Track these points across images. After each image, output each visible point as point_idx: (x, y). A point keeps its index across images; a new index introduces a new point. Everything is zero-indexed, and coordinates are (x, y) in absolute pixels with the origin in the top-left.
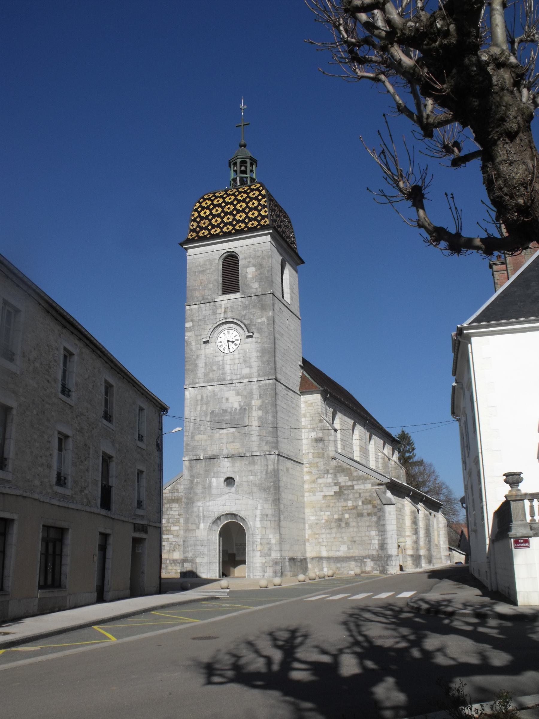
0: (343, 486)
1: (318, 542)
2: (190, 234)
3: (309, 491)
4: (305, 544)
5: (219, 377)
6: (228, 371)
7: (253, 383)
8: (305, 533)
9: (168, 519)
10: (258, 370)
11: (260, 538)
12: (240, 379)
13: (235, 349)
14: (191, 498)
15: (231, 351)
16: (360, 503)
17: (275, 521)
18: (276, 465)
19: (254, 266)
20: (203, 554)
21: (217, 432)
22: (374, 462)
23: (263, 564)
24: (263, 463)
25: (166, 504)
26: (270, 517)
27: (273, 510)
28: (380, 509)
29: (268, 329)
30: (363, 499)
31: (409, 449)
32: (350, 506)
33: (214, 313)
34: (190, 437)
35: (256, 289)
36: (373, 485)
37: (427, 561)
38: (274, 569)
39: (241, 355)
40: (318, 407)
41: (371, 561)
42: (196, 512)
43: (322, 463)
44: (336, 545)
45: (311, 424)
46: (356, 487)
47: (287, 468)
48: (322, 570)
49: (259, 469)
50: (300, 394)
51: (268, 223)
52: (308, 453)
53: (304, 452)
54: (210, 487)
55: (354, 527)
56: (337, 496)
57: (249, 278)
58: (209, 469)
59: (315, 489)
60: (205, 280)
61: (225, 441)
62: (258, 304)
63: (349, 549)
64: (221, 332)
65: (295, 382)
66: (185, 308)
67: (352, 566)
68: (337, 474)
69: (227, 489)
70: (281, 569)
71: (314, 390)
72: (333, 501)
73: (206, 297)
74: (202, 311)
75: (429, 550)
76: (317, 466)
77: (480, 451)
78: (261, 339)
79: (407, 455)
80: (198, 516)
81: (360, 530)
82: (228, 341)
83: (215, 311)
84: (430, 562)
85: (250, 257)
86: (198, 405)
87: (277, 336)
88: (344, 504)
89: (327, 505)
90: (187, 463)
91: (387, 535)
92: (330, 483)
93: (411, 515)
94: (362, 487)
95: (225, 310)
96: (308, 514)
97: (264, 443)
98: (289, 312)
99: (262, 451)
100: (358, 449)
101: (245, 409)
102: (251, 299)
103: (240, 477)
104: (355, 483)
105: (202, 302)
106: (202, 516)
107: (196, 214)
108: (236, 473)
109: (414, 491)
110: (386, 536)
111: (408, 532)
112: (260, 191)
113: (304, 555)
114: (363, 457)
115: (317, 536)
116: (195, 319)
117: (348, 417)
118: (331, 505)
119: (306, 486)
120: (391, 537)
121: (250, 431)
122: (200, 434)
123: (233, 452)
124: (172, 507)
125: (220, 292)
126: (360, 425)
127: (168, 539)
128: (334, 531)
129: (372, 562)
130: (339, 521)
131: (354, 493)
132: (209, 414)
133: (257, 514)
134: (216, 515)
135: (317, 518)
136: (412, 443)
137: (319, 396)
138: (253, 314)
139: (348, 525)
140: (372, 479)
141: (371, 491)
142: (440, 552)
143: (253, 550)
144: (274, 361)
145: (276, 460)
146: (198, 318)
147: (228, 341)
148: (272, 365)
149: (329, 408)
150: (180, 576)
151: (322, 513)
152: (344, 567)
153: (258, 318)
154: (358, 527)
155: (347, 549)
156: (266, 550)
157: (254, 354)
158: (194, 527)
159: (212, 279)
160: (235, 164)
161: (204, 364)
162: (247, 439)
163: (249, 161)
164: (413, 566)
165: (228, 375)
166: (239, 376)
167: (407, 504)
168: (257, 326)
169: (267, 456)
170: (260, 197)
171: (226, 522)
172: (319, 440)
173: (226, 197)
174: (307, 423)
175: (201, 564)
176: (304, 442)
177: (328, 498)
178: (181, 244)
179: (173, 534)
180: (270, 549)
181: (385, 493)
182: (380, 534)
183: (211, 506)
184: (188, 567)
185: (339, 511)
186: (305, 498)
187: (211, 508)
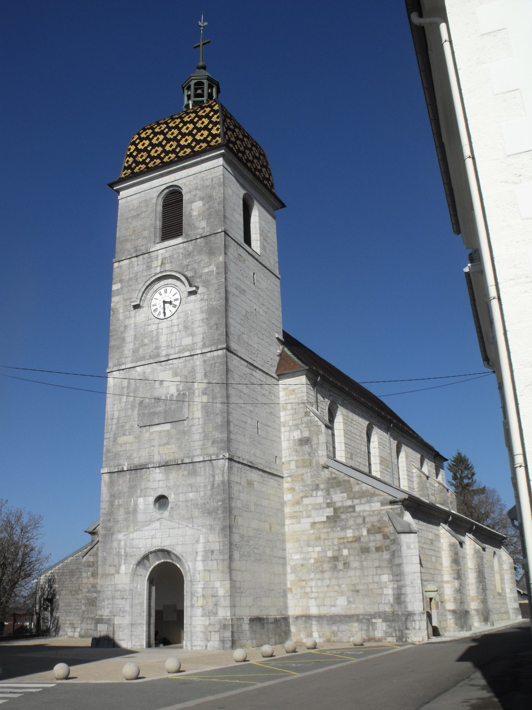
0: (340, 508)
1: (304, 592)
2: (124, 173)
4: (285, 596)
5: (152, 353)
7: (196, 357)
8: (285, 580)
10: (203, 338)
11: (202, 586)
12: (179, 352)
13: (173, 312)
14: (111, 528)
16: (365, 533)
17: (224, 560)
18: (226, 476)
19: (202, 199)
20: (124, 611)
21: (147, 431)
22: (406, 481)
23: (206, 627)
24: (207, 473)
26: (216, 555)
27: (222, 544)
28: (394, 540)
29: (218, 280)
30: (369, 525)
31: (467, 474)
32: (350, 537)
33: (149, 267)
34: (111, 439)
35: (203, 228)
36: (383, 504)
37: (482, 618)
38: (221, 636)
39: (181, 320)
40: (302, 394)
41: (383, 621)
43: (309, 474)
44: (330, 597)
46: (358, 509)
47: (248, 481)
48: (310, 635)
49: (203, 481)
50: (277, 377)
52: (290, 461)
53: (284, 460)
54: (135, 511)
55: (356, 568)
56: (331, 522)
58: (134, 485)
59: (300, 514)
60: (139, 226)
61: (156, 443)
62: (204, 249)
63: (349, 602)
64: (155, 292)
66: (113, 266)
67: (354, 630)
69: (157, 514)
70: (233, 636)
71: (295, 370)
72: (325, 530)
73: (139, 248)
74: (133, 267)
75: (484, 601)
77: (493, 292)
78: (208, 294)
79: (466, 481)
80: (119, 555)
81: (366, 574)
82: (165, 302)
83: (150, 264)
84: (486, 619)
85: (196, 189)
87: (231, 289)
88: (342, 534)
89: (316, 537)
90: (106, 477)
91: (404, 580)
92: (320, 504)
94: (367, 507)
95: (162, 261)
96: (290, 551)
97: (210, 443)
100: (378, 461)
101: (184, 394)
102: (196, 242)
103: (176, 494)
104: (356, 501)
105: (134, 255)
106: (123, 554)
108: (170, 489)
109: (477, 525)
111: (447, 574)
113: (283, 612)
115: (304, 583)
116: (124, 278)
117: (358, 415)
118: (323, 536)
119: (287, 510)
120: (412, 583)
121: (190, 426)
122: (124, 434)
126: (380, 428)
128: (327, 575)
129: (384, 624)
130: (334, 561)
131: (356, 517)
132: (137, 406)
134: (143, 552)
136: (471, 467)
137: (303, 379)
138: (199, 262)
139: (347, 566)
140: (382, 496)
141: (380, 513)
142: (506, 603)
143: (192, 606)
144: (224, 323)
145: (226, 467)
146: (128, 277)
147: (165, 302)
148: (223, 330)
149: (324, 398)
150: (92, 644)
151: (310, 549)
152: (342, 631)
153: (204, 267)
154: (362, 568)
155: (346, 603)
157: (199, 317)
158: (112, 570)
159: (148, 225)
160: (189, 88)
161: (133, 337)
163: (206, 82)
164: (457, 627)
165: (163, 348)
166: (177, 349)
167: (444, 533)
168: (203, 277)
169: (214, 462)
171: (157, 563)
174: (288, 418)
175: (120, 627)
176: (285, 445)
177: (318, 526)
178: (111, 185)
180: (216, 605)
181: (401, 515)
182: (395, 579)
183: (136, 539)
184: (102, 630)
185: (334, 545)
186: (286, 527)
187: (135, 542)
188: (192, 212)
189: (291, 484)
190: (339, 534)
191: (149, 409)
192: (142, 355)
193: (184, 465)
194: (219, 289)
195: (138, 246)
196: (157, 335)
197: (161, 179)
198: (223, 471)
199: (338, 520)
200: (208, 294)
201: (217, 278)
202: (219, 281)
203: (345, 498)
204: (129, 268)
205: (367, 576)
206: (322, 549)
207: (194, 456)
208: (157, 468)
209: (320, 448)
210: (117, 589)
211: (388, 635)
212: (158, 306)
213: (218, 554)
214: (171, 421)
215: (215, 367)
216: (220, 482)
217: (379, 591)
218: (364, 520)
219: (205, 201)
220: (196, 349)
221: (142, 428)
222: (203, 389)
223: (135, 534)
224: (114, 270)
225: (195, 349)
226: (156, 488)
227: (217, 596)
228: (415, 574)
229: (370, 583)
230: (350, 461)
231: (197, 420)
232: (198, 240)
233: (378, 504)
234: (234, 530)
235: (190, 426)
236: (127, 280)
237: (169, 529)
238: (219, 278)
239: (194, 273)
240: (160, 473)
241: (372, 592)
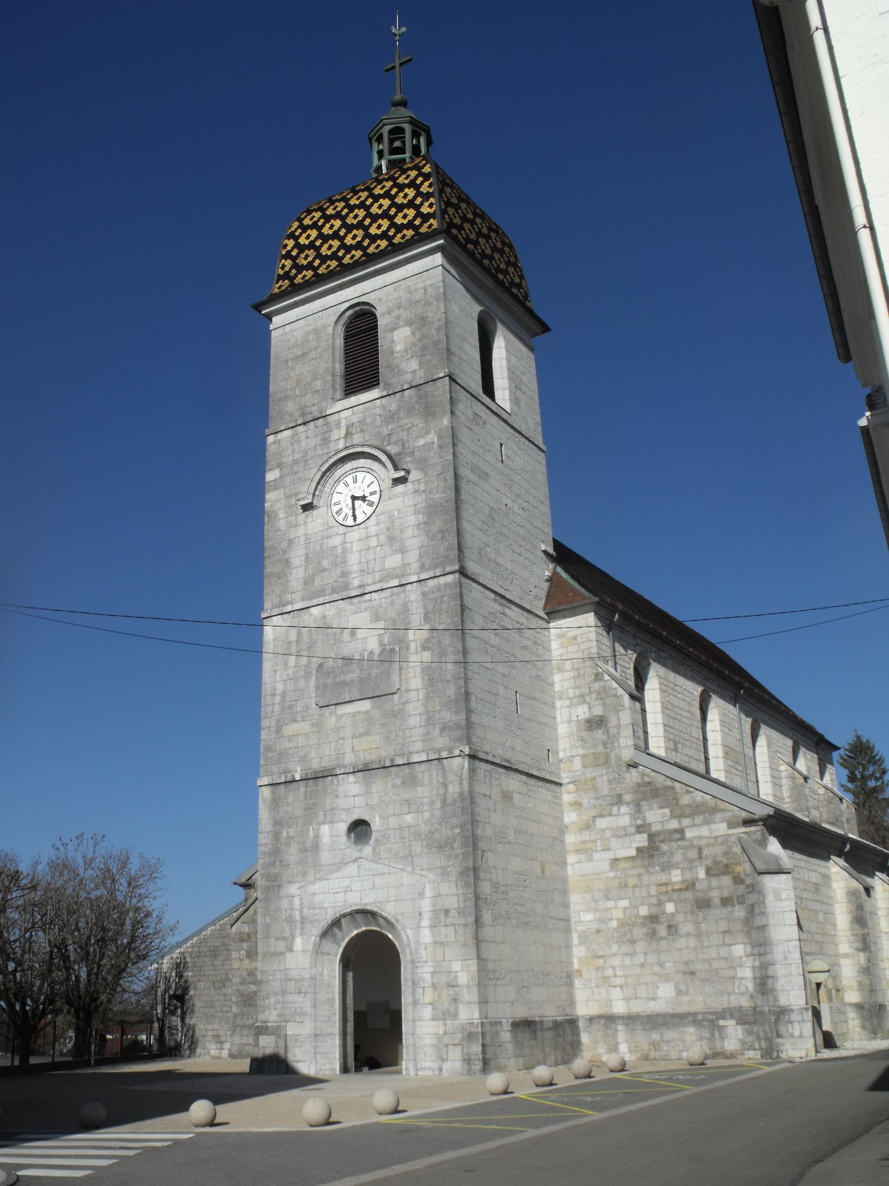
0: (658, 833)
1: (603, 977)
2: (277, 286)
3: (577, 851)
5: (336, 584)
7: (409, 587)
8: (570, 956)
10: (421, 556)
11: (430, 970)
12: (381, 581)
14: (277, 876)
15: (359, 521)
16: (702, 874)
17: (466, 925)
18: (465, 784)
19: (409, 323)
21: (331, 713)
22: (769, 785)
23: (439, 1038)
24: (435, 781)
26: (454, 918)
27: (461, 899)
29: (441, 457)
30: (708, 862)
31: (874, 772)
32: (677, 883)
33: (325, 441)
34: (273, 729)
35: (414, 372)
36: (731, 825)
38: (465, 1051)
39: (382, 526)
41: (737, 1024)
42: (286, 911)
43: (605, 778)
44: (646, 984)
45: (576, 688)
46: (689, 834)
48: (614, 1049)
49: (427, 794)
50: (546, 617)
52: (573, 756)
53: (561, 755)
54: (316, 847)
55: (688, 935)
57: (397, 352)
58: (314, 804)
59: (592, 845)
61: (348, 732)
62: (417, 406)
63: (679, 992)
64: (338, 481)
65: (531, 587)
66: (265, 440)
67: (688, 1038)
68: (642, 803)
69: (353, 851)
70: (484, 1051)
71: (576, 604)
72: (634, 872)
73: (308, 410)
76: (595, 788)
79: (872, 784)
80: (290, 920)
81: (706, 943)
82: (354, 498)
85: (399, 308)
87: (464, 472)
88: (664, 878)
90: (266, 793)
91: (771, 953)
92: (625, 828)
93: (849, 902)
94: (704, 831)
96: (577, 908)
97: (437, 731)
98: (508, 428)
99: (432, 749)
100: (721, 753)
101: (392, 651)
103: (381, 817)
104: (686, 822)
105: (300, 422)
106: (298, 919)
108: (373, 809)
110: (769, 957)
114: (736, 772)
115: (601, 961)
116: (285, 460)
117: (685, 676)
118: (632, 882)
119: (570, 839)
120: (785, 958)
121: (404, 704)
122: (294, 720)
123: (368, 758)
125: (339, 394)
126: (722, 697)
128: (640, 947)
129: (739, 1028)
130: (652, 922)
131: (685, 848)
132: (314, 672)
133: (424, 909)
134: (330, 916)
135: (597, 915)
137: (590, 618)
139: (673, 930)
140: (729, 811)
143: (415, 1003)
146: (291, 458)
147: (354, 498)
149: (625, 649)
151: (610, 904)
152: (668, 1041)
154: (699, 935)
155: (674, 993)
157: (412, 520)
158: (281, 946)
160: (380, 139)
161: (303, 557)
162: (397, 723)
163: (408, 128)
164: (865, 1033)
166: (377, 576)
167: (837, 873)
168: (417, 454)
169: (445, 761)
171: (355, 932)
172: (596, 723)
175: (296, 1040)
176: (562, 730)
177: (623, 865)
178: (258, 307)
180: (455, 1000)
181: (763, 843)
182: (756, 951)
183: (319, 894)
184: (267, 1045)
185: (650, 896)
186: (569, 868)
187: (317, 899)
188: (393, 345)
189: (575, 794)
190: (659, 878)
191: (335, 677)
193: (395, 768)
195: (306, 406)
196: (343, 552)
198: (461, 776)
199: (656, 853)
201: (439, 454)
203: (667, 816)
205: (708, 947)
208: (349, 775)
209: (622, 734)
210: (289, 977)
211: (747, 1047)
212: (343, 505)
213: (456, 915)
215: (442, 602)
216: (456, 795)
217: (730, 973)
219: (414, 326)
220: (410, 574)
221: (323, 709)
222: (423, 641)
223: (317, 886)
224: (268, 448)
225: (407, 575)
226: (349, 809)
227: (457, 986)
229: (713, 959)
230: (674, 754)
231: (415, 692)
232: (406, 392)
234: (482, 875)
235: (404, 704)
236: (290, 463)
237: (374, 875)
239: (401, 447)
241: (717, 974)
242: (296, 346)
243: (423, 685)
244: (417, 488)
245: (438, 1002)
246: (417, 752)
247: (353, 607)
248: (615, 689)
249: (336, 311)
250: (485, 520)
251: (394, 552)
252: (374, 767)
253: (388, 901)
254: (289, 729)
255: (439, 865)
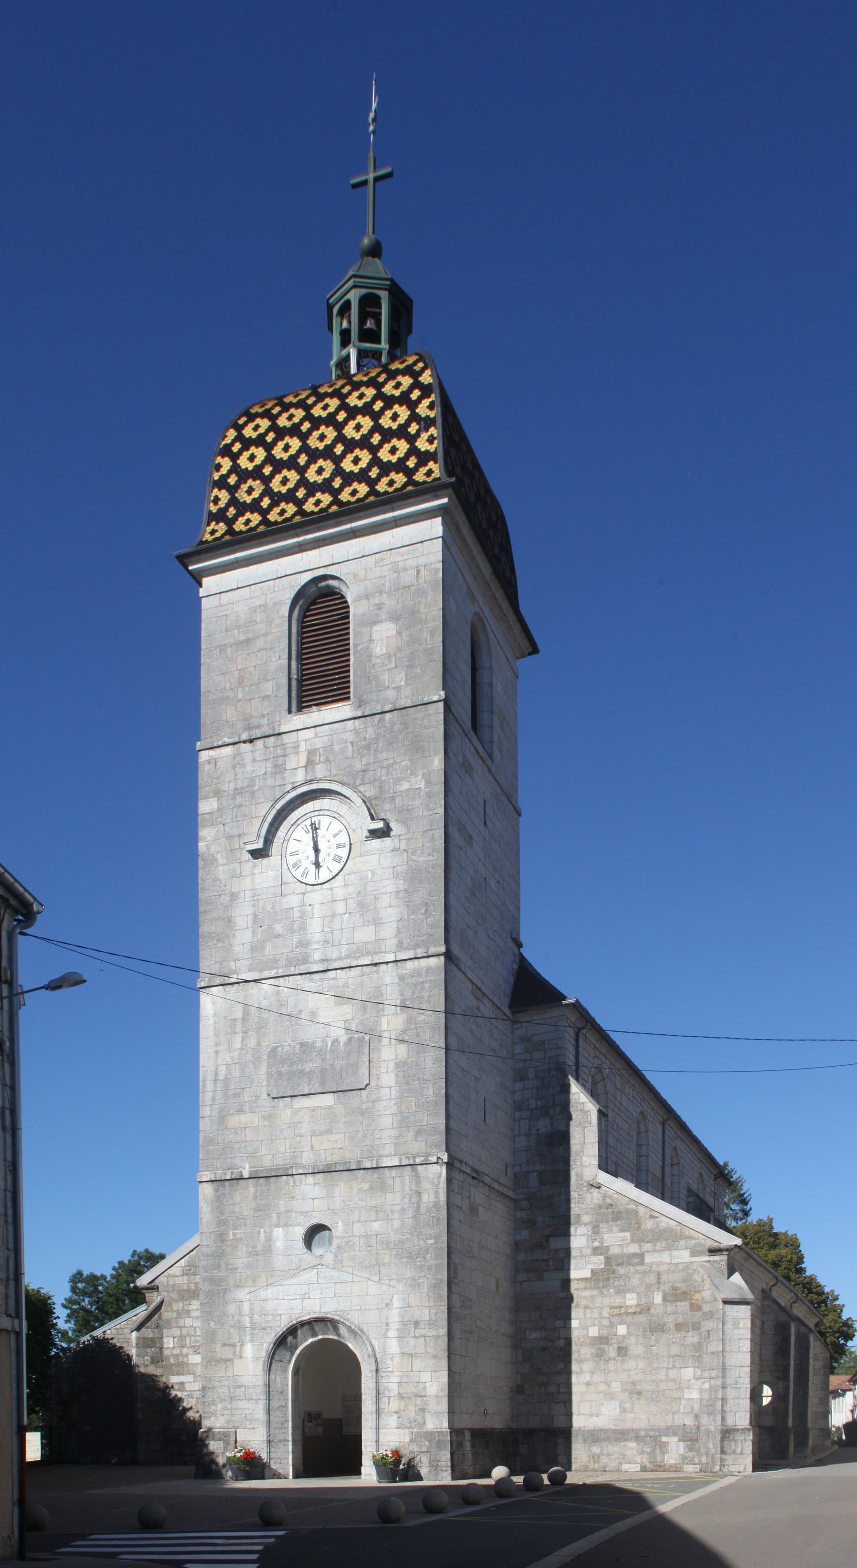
0: (617, 1256)
2: (209, 529)
5: (291, 955)
6: (317, 937)
7: (383, 967)
9: (182, 1337)
10: (399, 931)
11: (397, 1380)
12: (348, 957)
14: (221, 1279)
16: (658, 1299)
19: (394, 618)
21: (286, 1106)
24: (407, 1189)
25: (176, 1301)
29: (429, 809)
30: (667, 1288)
32: (631, 1306)
33: (279, 769)
35: (398, 689)
36: (693, 1254)
39: (351, 889)
41: (680, 1440)
42: (233, 1317)
46: (648, 1259)
51: (437, 474)
54: (268, 1250)
57: (377, 657)
58: (266, 1205)
60: (252, 669)
61: (305, 1129)
62: (401, 737)
63: (623, 1410)
67: (629, 1453)
69: (308, 1258)
73: (254, 722)
78: (408, 839)
80: (240, 1327)
85: (381, 592)
86: (235, 1033)
88: (618, 1301)
90: (207, 1191)
94: (665, 1257)
97: (412, 1134)
104: (648, 1246)
105: (244, 737)
106: (248, 1325)
107: (226, 464)
108: (336, 1213)
112: (415, 375)
120: (736, 1383)
121: (374, 1101)
122: (241, 1111)
124: (190, 1308)
127: (182, 1384)
129: (681, 1444)
132: (265, 1057)
139: (623, 1352)
140: (693, 1238)
146: (232, 786)
156: (412, 1412)
157: (389, 886)
158: (227, 1353)
161: (250, 918)
165: (315, 946)
168: (398, 800)
169: (419, 1167)
170: (415, 394)
171: (311, 1340)
173: (315, 404)
178: (184, 560)
179: (193, 1374)
187: (270, 1305)
188: (372, 646)
189: (528, 1212)
190: (612, 1301)
191: (291, 1065)
192: (271, 957)
193: (362, 1171)
194: (431, 830)
195: (252, 716)
196: (301, 917)
197: (300, 555)
198: (438, 1185)
199: (612, 1276)
200: (408, 839)
201: (427, 805)
202: (431, 813)
203: (627, 1240)
204: (234, 767)
205: (657, 1369)
206: (580, 1324)
207: (382, 1156)
208: (308, 1175)
209: (586, 1153)
210: (238, 1384)
211: (686, 1461)
212: (301, 857)
213: (427, 1326)
214: (335, 1090)
215: (422, 989)
216: (431, 1205)
217: (678, 1394)
218: (659, 1278)
219: (401, 623)
220: (384, 952)
221: (276, 1100)
222: (398, 1032)
223: (269, 1291)
224: (201, 769)
225: (381, 952)
226: (308, 1212)
227: (425, 1396)
228: (742, 1369)
229: (662, 1381)
231: (387, 1090)
232: (388, 716)
233: (686, 1253)
235: (374, 1101)
236: (231, 793)
237: (335, 1283)
238: (431, 805)
239: (377, 789)
240: (314, 1185)
241: (663, 1394)
242: (238, 627)
243: (397, 1083)
244: (397, 846)
245: (404, 1411)
246: (388, 1156)
247: (313, 984)
248: (583, 1103)
249: (293, 584)
250: (468, 896)
251: (366, 923)
252: (337, 1169)
253: (351, 1310)
254: (234, 1121)
255: (409, 1276)
